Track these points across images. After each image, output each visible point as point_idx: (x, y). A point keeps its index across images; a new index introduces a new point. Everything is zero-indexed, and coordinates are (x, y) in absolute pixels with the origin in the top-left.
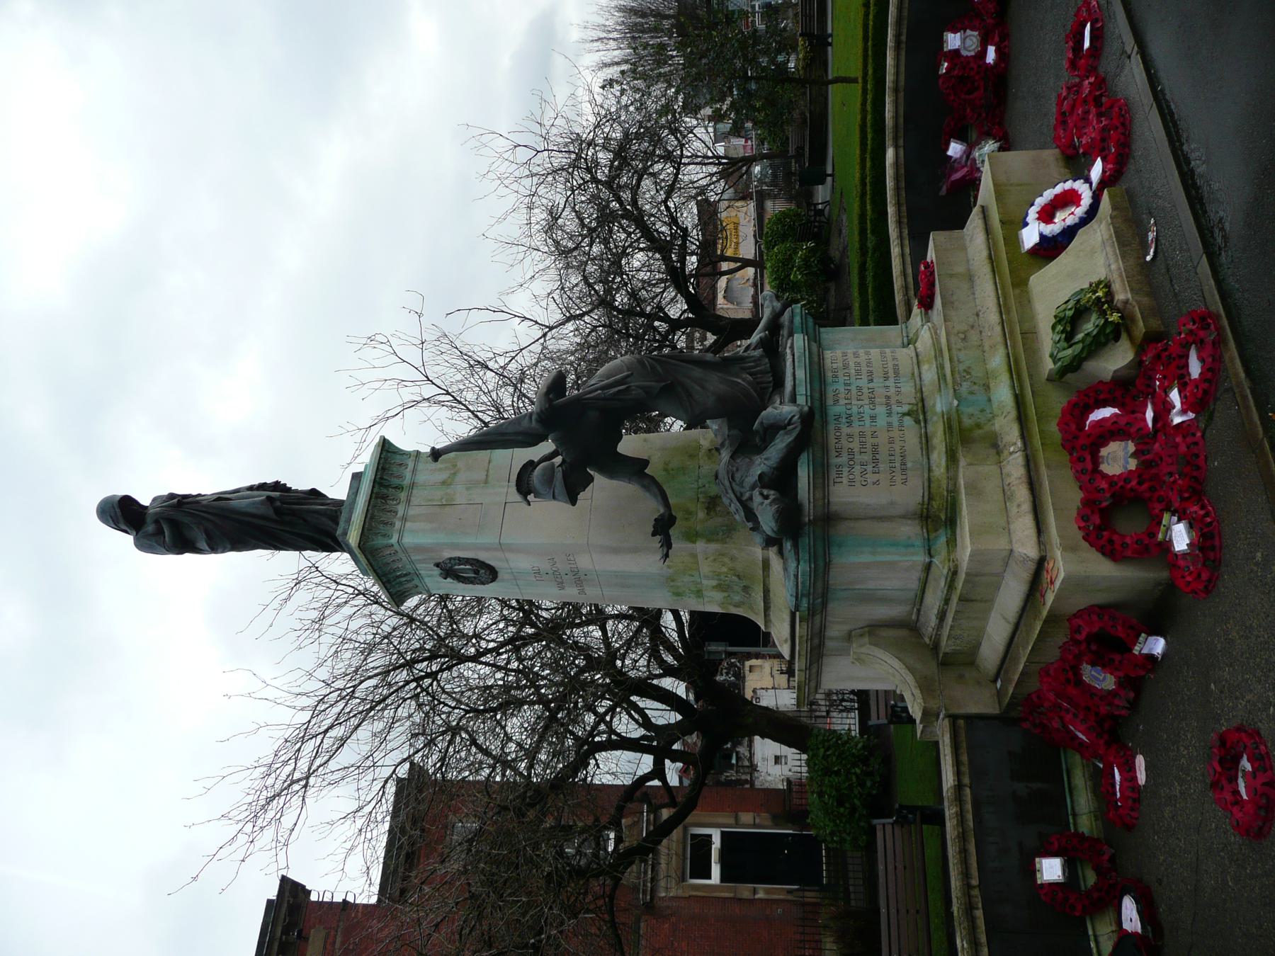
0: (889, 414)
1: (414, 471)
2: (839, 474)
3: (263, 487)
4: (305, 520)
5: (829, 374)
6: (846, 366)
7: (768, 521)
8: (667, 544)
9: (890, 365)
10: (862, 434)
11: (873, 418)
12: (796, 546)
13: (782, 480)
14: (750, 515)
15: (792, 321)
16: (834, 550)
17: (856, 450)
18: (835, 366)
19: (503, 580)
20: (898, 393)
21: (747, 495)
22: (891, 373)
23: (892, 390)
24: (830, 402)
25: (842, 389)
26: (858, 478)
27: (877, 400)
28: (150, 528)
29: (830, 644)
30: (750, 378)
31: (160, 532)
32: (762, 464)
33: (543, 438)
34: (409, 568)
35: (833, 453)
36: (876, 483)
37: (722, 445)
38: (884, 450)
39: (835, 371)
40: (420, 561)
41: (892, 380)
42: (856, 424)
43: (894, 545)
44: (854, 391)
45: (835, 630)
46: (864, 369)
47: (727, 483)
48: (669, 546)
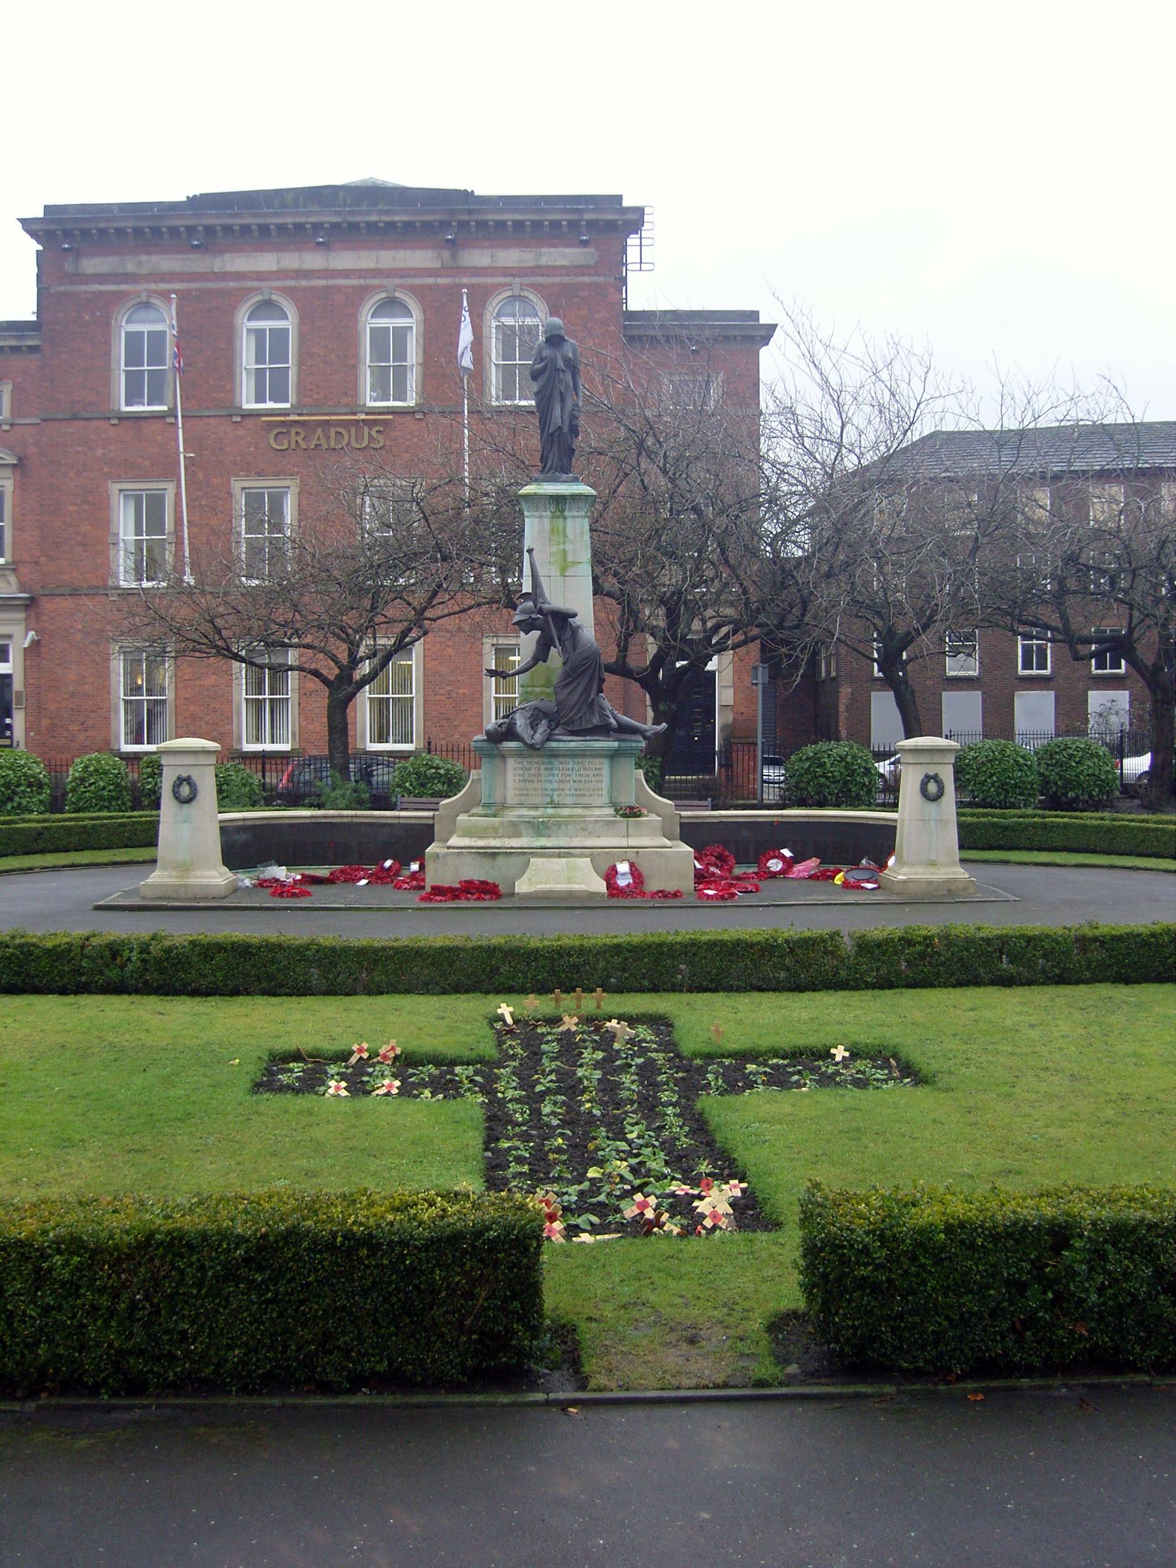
1: (574, 517)
6: (585, 769)
10: (540, 775)
24: (561, 760)
25: (570, 766)
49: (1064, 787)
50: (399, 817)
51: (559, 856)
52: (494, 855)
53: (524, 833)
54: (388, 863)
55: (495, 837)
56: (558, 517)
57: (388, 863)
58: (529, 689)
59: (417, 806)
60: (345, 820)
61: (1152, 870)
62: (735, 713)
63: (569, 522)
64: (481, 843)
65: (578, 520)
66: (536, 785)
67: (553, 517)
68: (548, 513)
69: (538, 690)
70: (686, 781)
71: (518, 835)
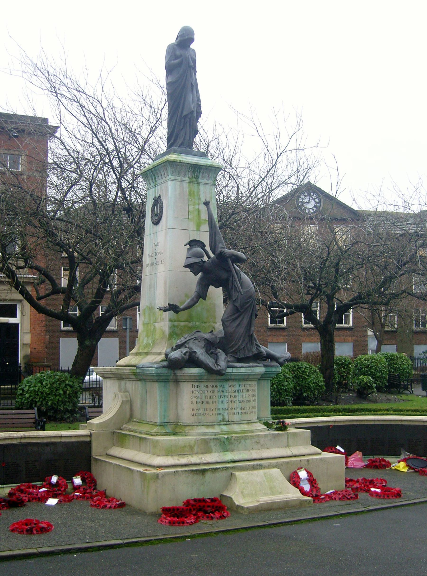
0: (224, 409)
1: (205, 184)
2: (196, 387)
3: (199, 106)
4: (182, 129)
5: (243, 383)
6: (247, 391)
7: (176, 354)
8: (166, 310)
9: (247, 411)
10: (214, 397)
11: (222, 402)
12: (164, 367)
13: (192, 361)
14: (179, 347)
15: (272, 366)
16: (163, 384)
17: (207, 394)
18: (248, 386)
19: (153, 228)
20: (234, 414)
21: (187, 346)
22: (243, 411)
23: (235, 411)
24: (230, 383)
25: (237, 388)
26: (194, 395)
27: (231, 404)
28: (178, 53)
29: (123, 383)
30: (242, 347)
31: (176, 57)
32: (201, 354)
33: (214, 253)
34: (158, 182)
35: (206, 384)
36: (192, 403)
37: (213, 334)
38: (207, 406)
39: (245, 386)
40: (161, 188)
41: (240, 411)
42: (219, 394)
43: (165, 411)
44: (235, 394)
45: (129, 385)
46: (246, 399)
47: (193, 337)
48: (165, 311)
49: (301, 390)
50: (61, 437)
51: (254, 468)
52: (203, 472)
53: (214, 449)
54: (54, 479)
55: (192, 454)
56: (193, 183)
57: (54, 479)
58: (176, 323)
59: (22, 421)
60: (15, 442)
61: (17, 414)
62: (32, 348)
63: (202, 187)
64: (184, 461)
65: (207, 186)
66: (212, 406)
67: (190, 182)
68: (187, 179)
69: (182, 324)
70: (8, 389)
71: (208, 451)
